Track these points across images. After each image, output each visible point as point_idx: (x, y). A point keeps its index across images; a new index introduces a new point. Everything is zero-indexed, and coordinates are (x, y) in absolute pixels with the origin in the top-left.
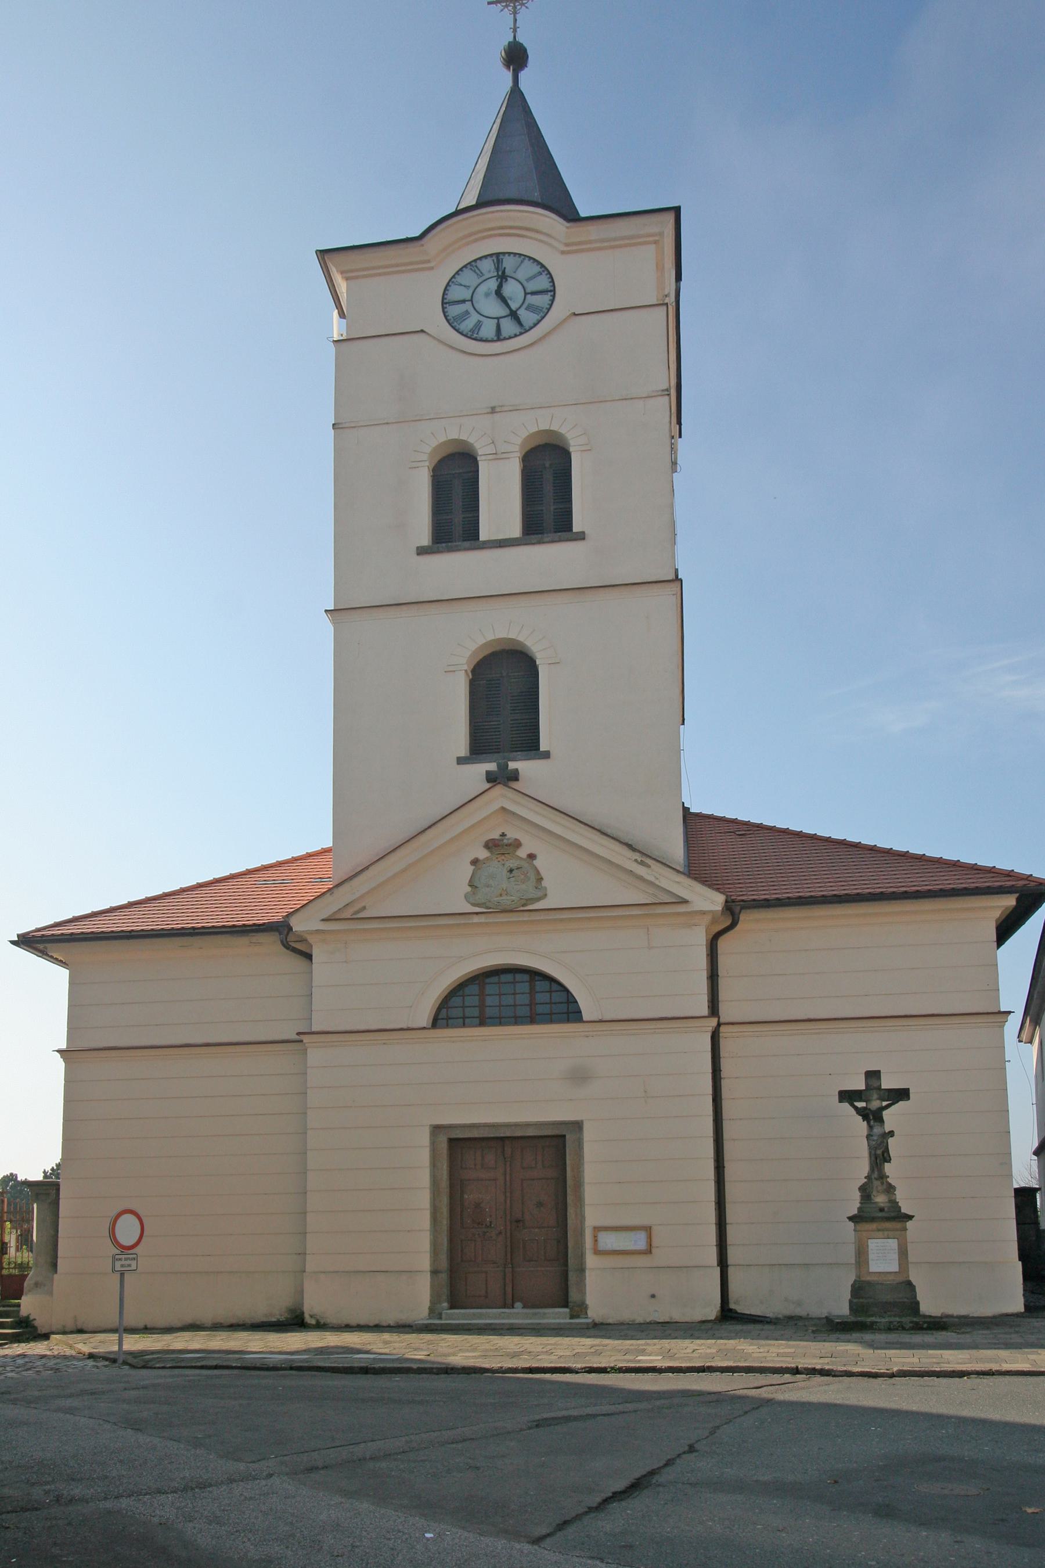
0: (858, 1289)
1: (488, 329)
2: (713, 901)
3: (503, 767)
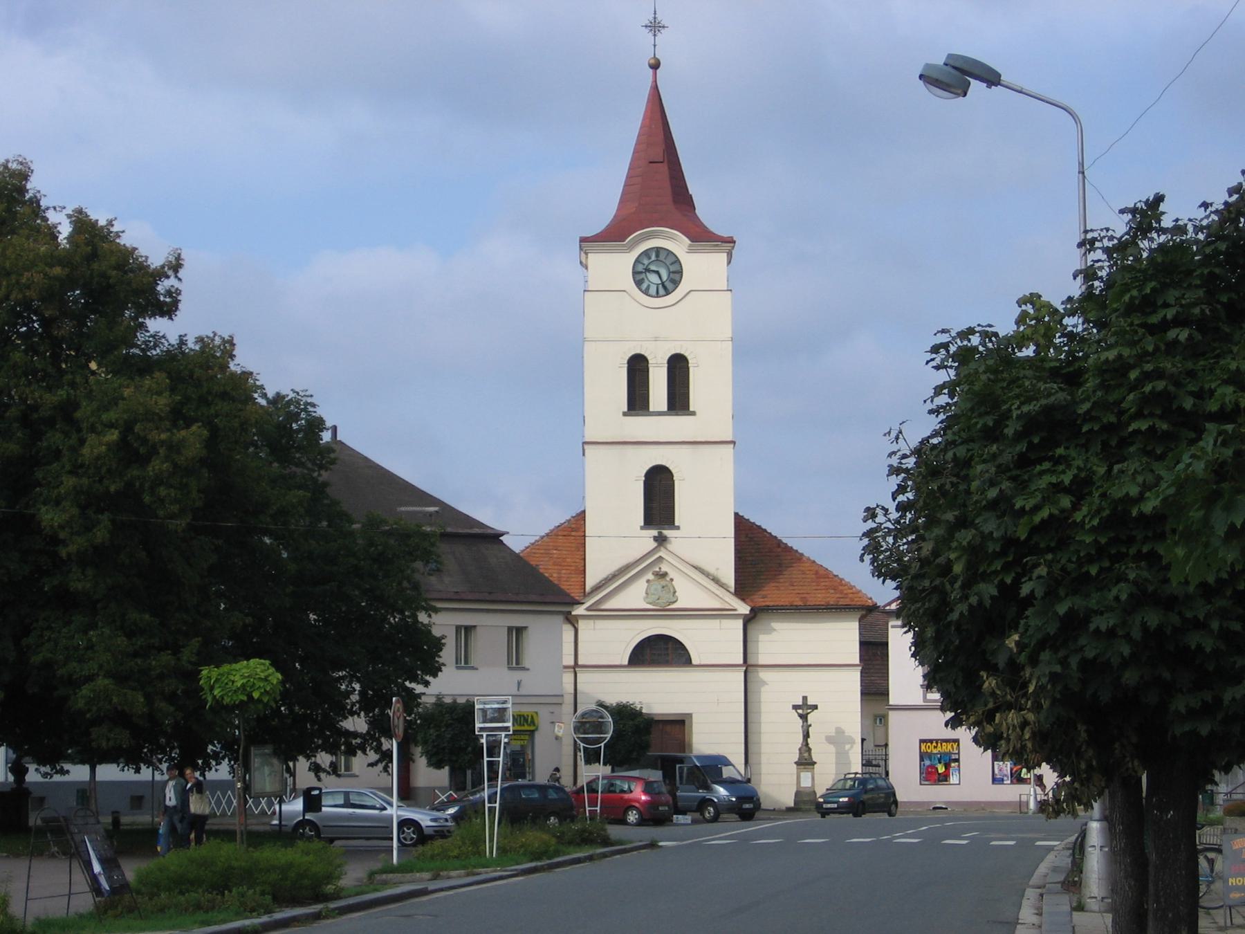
0: (797, 794)
1: (653, 290)
2: (744, 609)
3: (660, 533)
